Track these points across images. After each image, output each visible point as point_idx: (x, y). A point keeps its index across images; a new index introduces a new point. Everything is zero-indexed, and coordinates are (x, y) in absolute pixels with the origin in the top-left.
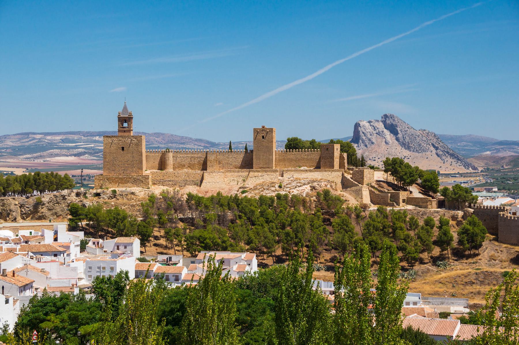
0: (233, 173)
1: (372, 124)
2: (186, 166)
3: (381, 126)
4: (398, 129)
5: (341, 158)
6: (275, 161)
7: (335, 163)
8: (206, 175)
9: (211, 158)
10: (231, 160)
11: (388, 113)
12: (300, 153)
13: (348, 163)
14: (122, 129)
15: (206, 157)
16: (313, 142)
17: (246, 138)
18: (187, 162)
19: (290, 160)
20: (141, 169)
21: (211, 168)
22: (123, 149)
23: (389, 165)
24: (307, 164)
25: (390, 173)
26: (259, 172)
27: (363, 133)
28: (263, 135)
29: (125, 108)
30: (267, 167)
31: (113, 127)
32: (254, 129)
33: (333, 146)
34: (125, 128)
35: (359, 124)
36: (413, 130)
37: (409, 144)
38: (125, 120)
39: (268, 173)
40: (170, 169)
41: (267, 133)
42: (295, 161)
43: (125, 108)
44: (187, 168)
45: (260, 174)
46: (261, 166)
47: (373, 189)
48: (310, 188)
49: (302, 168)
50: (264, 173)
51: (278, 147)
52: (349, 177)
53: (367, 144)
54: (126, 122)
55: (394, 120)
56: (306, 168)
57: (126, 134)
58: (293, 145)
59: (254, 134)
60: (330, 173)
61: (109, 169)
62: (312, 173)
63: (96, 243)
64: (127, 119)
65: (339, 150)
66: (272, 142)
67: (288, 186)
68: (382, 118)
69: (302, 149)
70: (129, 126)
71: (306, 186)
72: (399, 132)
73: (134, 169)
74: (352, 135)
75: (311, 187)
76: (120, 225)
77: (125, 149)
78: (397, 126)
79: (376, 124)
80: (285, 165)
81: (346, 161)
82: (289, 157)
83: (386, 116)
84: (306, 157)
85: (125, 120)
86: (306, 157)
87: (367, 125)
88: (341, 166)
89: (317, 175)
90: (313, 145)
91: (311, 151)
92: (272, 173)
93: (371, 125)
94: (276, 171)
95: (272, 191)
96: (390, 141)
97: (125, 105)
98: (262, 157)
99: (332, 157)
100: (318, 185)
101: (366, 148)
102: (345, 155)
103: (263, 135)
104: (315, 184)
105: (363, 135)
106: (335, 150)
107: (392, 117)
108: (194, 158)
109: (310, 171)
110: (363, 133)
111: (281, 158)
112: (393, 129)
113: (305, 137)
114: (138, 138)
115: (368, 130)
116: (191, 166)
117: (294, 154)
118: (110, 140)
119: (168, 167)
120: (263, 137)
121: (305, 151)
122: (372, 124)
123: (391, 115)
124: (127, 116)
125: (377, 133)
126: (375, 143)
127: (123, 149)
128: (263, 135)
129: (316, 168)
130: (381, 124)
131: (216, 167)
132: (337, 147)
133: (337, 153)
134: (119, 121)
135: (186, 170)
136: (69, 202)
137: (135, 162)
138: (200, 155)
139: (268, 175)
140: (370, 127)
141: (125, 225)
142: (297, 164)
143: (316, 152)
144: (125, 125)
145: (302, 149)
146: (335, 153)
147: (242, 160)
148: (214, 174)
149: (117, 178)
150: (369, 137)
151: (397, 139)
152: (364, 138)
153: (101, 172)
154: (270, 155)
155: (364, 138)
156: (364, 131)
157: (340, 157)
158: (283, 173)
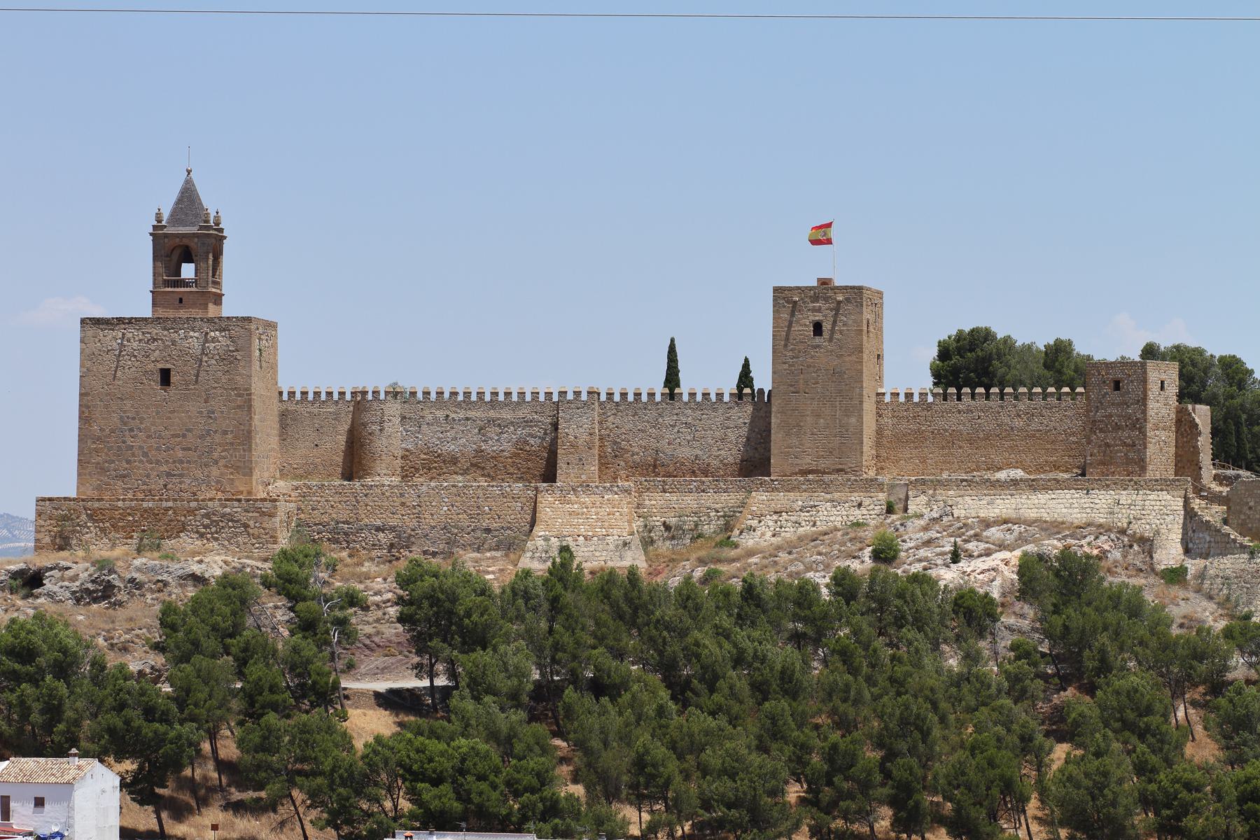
5: (1185, 427)
6: (878, 444)
7: (1151, 450)
12: (995, 403)
15: (555, 426)
16: (1058, 354)
17: (731, 345)
19: (949, 440)
20: (246, 470)
21: (573, 471)
22: (165, 377)
24: (1028, 459)
28: (822, 320)
29: (188, 199)
30: (831, 471)
32: (776, 290)
34: (184, 283)
38: (186, 248)
40: (384, 477)
41: (837, 310)
42: (971, 441)
43: (188, 199)
44: (465, 472)
49: (1002, 475)
51: (906, 367)
54: (190, 261)
56: (1019, 473)
58: (970, 363)
59: (776, 311)
61: (103, 470)
64: (193, 244)
65: (1173, 389)
66: (860, 350)
67: (923, 553)
69: (1002, 386)
71: (1005, 555)
73: (215, 472)
77: (174, 378)
80: (924, 461)
81: (1205, 442)
82: (941, 423)
84: (1018, 423)
85: (186, 248)
86: (1018, 423)
88: (1186, 463)
90: (1059, 364)
91: (1045, 395)
94: (871, 485)
99: (1138, 425)
102: (1202, 415)
103: (822, 320)
106: (1153, 388)
108: (501, 425)
111: (904, 426)
113: (1029, 329)
117: (973, 408)
119: (380, 467)
120: (818, 329)
124: (194, 230)
127: (165, 377)
128: (818, 317)
132: (1165, 377)
133: (1161, 403)
134: (156, 258)
137: (218, 438)
142: (975, 461)
144: (188, 271)
145: (1002, 386)
146: (1151, 405)
147: (744, 431)
154: (847, 413)
157: (1179, 422)
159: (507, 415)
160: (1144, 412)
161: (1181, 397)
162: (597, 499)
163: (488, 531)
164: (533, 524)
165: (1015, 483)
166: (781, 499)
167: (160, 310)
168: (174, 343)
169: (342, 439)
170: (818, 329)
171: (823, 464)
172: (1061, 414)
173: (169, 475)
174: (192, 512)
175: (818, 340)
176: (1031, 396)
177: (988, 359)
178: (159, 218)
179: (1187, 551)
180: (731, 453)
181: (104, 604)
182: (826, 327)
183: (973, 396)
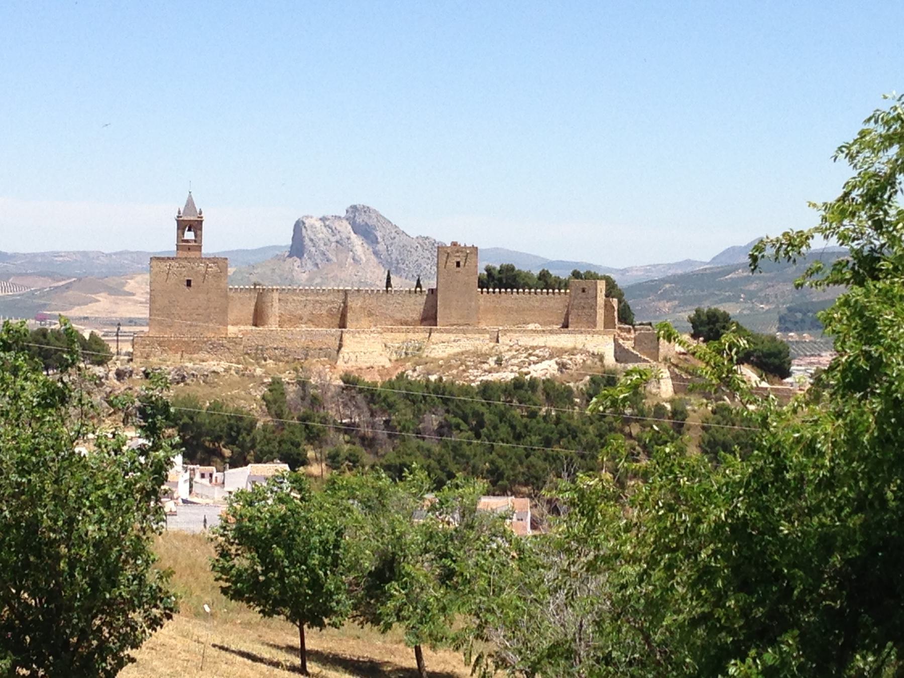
0: (398, 334)
1: (327, 223)
2: (305, 319)
3: (345, 228)
4: (379, 234)
5: (608, 307)
8: (346, 337)
9: (355, 303)
10: (391, 307)
11: (359, 201)
13: (619, 320)
14: (183, 245)
18: (305, 313)
22: (189, 283)
23: (702, 324)
25: (701, 339)
26: (448, 332)
27: (312, 240)
29: (190, 204)
31: (166, 241)
33: (596, 283)
34: (187, 241)
35: (304, 223)
36: (405, 237)
37: (398, 263)
38: (190, 224)
39: (469, 335)
40: (272, 325)
42: (516, 312)
43: (190, 204)
44: (306, 323)
45: (452, 337)
46: (453, 321)
47: (676, 370)
48: (556, 367)
49: (531, 326)
50: (461, 335)
52: (628, 345)
53: (319, 261)
54: (189, 230)
55: (370, 217)
57: (192, 254)
60: (589, 337)
62: (555, 337)
63: (207, 475)
68: (347, 211)
70: (198, 236)
72: (380, 240)
74: (290, 243)
75: (557, 363)
76: (244, 440)
78: (375, 229)
79: (336, 224)
80: (497, 320)
83: (354, 208)
84: (537, 304)
85: (190, 224)
86: (537, 304)
87: (319, 224)
89: (565, 340)
92: (477, 336)
93: (325, 226)
95: (485, 371)
96: (363, 257)
97: (190, 196)
98: (455, 303)
99: (593, 307)
100: (571, 359)
101: (315, 269)
102: (615, 302)
104: (565, 359)
105: (310, 244)
106: (599, 291)
107: (366, 210)
109: (551, 332)
110: (312, 240)
112: (366, 232)
114: (220, 262)
115: (320, 236)
116: (314, 320)
118: (164, 266)
120: (458, 264)
121: (536, 293)
122: (327, 223)
123: (364, 207)
125: (337, 242)
126: (335, 259)
127: (189, 283)
128: (458, 260)
129: (562, 327)
130: (345, 223)
131: (364, 322)
135: (304, 327)
136: (108, 390)
137: (213, 310)
138: (331, 297)
139: (468, 339)
140: (324, 230)
141: (253, 440)
143: (557, 296)
145: (530, 289)
148: (363, 336)
149: (179, 341)
150: (323, 248)
151: (376, 253)
152: (313, 249)
153: (146, 329)
155: (313, 249)
156: (313, 237)
157: (606, 305)
158: (498, 337)
159: (323, 298)
160: (596, 302)
161: (606, 296)
162: (368, 336)
163: (321, 349)
164: (340, 346)
165: (535, 331)
166: (445, 336)
167: (180, 252)
168: (193, 268)
169: (253, 308)
170: (458, 264)
171: (460, 322)
172: (555, 301)
173: (191, 326)
174: (205, 342)
175: (458, 269)
176: (542, 293)
177: (515, 275)
178: (179, 213)
179: (617, 360)
180: (416, 316)
181: (182, 384)
182: (462, 264)
183: (518, 292)
